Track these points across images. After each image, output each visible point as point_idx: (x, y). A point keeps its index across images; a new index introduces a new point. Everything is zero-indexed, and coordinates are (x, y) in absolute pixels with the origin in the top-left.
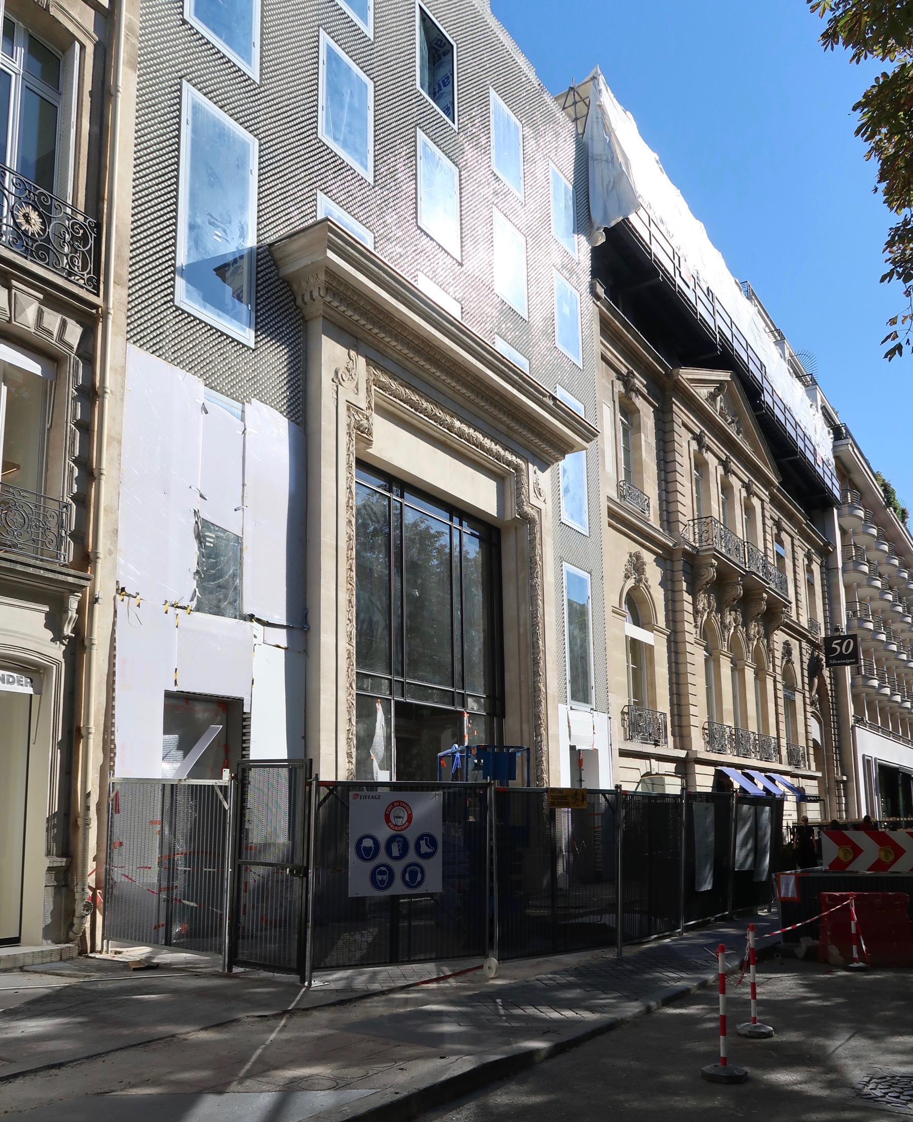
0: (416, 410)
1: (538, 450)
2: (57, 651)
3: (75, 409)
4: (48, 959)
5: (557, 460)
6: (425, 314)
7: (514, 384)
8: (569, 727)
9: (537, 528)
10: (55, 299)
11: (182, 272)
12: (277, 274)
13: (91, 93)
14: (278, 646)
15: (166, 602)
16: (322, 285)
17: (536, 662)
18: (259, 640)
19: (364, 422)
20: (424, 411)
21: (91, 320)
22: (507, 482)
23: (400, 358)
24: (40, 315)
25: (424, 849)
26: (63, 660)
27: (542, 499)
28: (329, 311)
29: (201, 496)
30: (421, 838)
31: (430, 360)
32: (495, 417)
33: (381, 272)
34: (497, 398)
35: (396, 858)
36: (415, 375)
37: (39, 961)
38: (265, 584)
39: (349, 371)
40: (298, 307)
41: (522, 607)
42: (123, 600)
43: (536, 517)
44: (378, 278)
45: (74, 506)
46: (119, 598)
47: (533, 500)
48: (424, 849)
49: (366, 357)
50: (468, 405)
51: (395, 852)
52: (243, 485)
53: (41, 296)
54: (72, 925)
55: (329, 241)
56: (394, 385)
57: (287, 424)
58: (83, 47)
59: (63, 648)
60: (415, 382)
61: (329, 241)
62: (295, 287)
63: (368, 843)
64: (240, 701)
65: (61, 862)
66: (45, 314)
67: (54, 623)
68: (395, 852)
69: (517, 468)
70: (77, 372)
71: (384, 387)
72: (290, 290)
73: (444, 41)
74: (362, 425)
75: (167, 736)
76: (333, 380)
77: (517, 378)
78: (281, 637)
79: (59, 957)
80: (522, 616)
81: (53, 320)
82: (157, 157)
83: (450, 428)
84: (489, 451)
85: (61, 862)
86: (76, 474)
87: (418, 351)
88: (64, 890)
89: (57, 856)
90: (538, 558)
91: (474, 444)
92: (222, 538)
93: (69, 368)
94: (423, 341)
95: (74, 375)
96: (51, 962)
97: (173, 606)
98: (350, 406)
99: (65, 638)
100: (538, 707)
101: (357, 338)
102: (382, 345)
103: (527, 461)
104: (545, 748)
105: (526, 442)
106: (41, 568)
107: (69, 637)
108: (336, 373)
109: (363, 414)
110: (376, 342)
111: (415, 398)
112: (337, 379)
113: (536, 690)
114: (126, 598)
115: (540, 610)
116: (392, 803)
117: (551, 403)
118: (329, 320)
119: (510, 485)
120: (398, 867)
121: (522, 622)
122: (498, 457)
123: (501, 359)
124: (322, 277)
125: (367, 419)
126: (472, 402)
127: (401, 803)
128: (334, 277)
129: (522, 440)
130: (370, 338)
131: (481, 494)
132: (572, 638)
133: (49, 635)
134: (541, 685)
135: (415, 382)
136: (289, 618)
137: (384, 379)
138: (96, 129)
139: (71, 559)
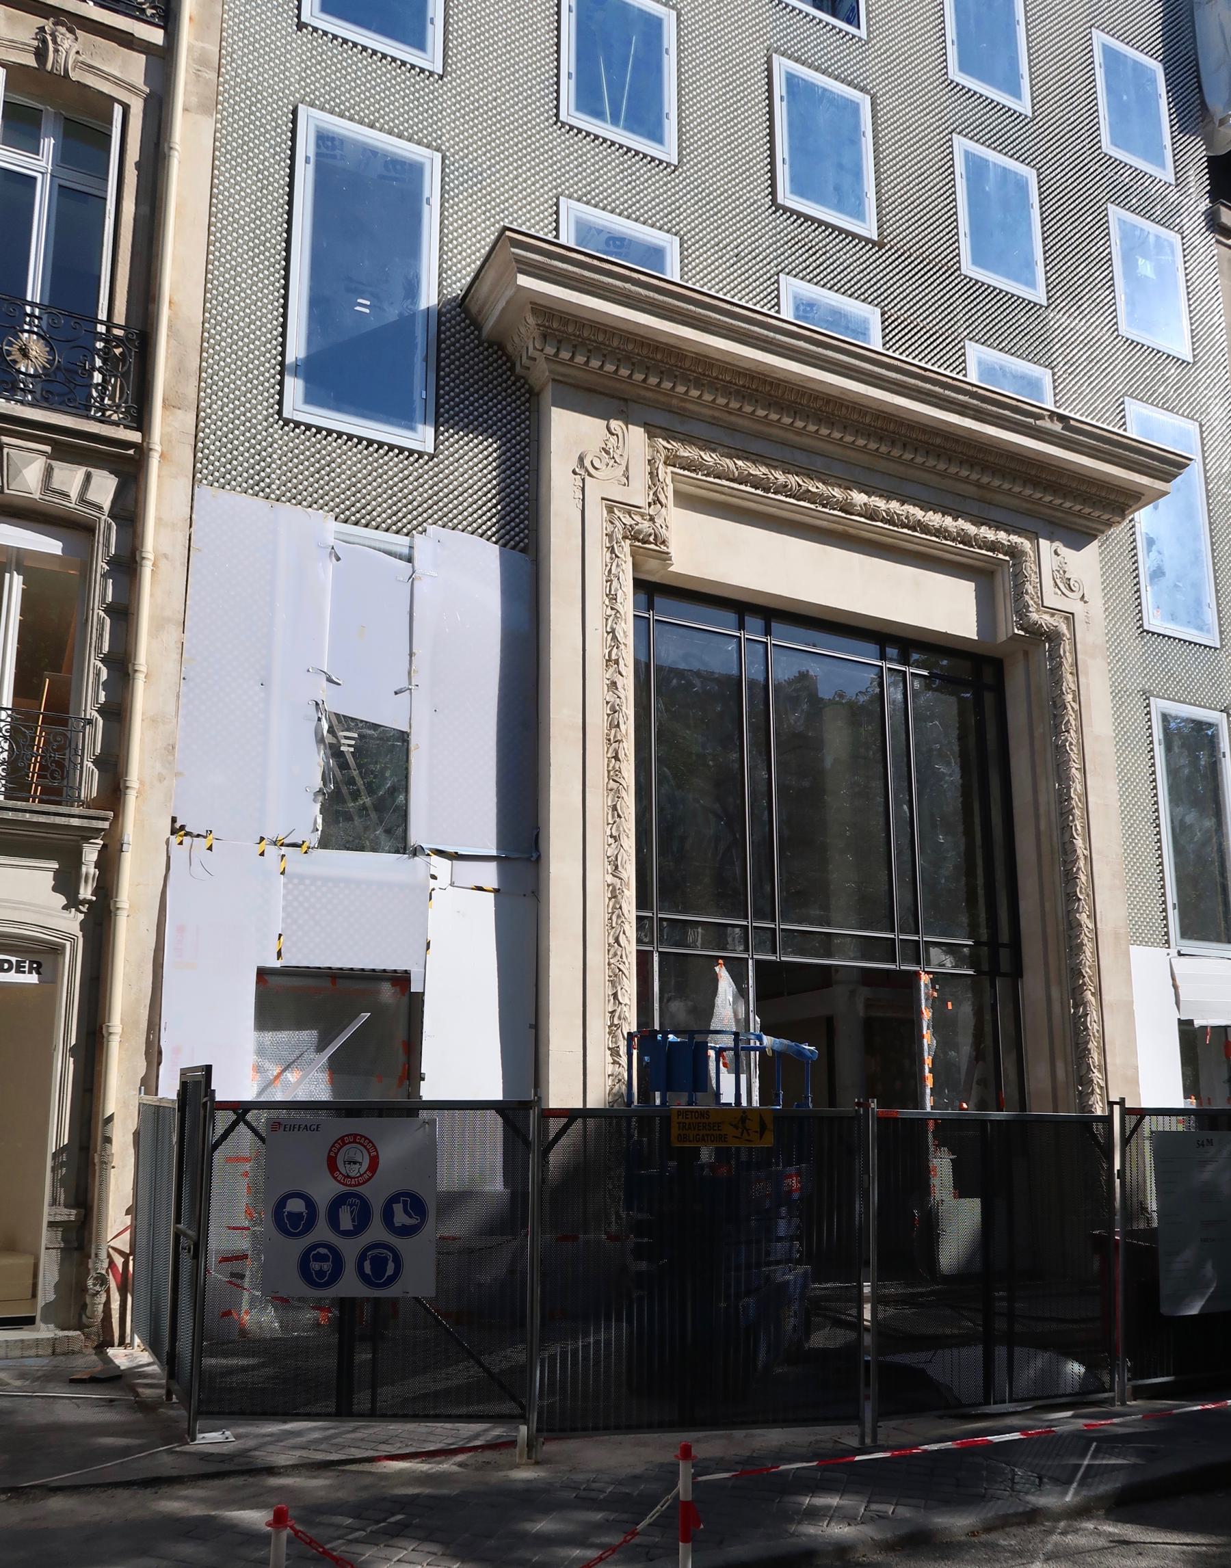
0: (767, 490)
1: (1059, 514)
2: (71, 923)
3: (105, 589)
4: (32, 1352)
5: (1109, 524)
6: (736, 332)
7: (962, 409)
8: (1175, 987)
9: (1066, 647)
10: (68, 448)
11: (297, 370)
12: (477, 338)
13: (138, 165)
14: (480, 889)
15: (262, 839)
16: (536, 333)
17: (1070, 878)
18: (444, 880)
19: (645, 526)
20: (783, 489)
21: (130, 468)
22: (993, 578)
23: (717, 414)
24: (48, 472)
25: (400, 1218)
26: (80, 934)
27: (1078, 595)
29: (330, 680)
30: (394, 1199)
31: (774, 403)
32: (943, 475)
33: (628, 286)
34: (938, 441)
35: (346, 1234)
36: (757, 436)
37: (17, 1353)
39: (607, 453)
40: (518, 378)
41: (1042, 785)
42: (181, 843)
43: (1063, 628)
44: (627, 296)
45: (100, 722)
46: (175, 840)
47: (1052, 600)
48: (400, 1218)
49: (647, 426)
50: (882, 465)
51: (346, 1222)
52: (411, 655)
53: (48, 449)
54: (84, 1306)
55: (517, 261)
56: (709, 458)
57: (498, 553)
58: (126, 108)
59: (82, 916)
61: (517, 261)
62: (510, 349)
63: (296, 1206)
65: (71, 1215)
66: (56, 472)
67: (66, 883)
68: (346, 1222)
69: (1014, 553)
70: (108, 540)
71: (689, 466)
72: (505, 354)
74: (640, 532)
75: (269, 1036)
76: (574, 472)
77: (966, 399)
78: (489, 874)
79: (50, 1351)
80: (1043, 799)
81: (70, 478)
82: (709, 273)
83: (847, 508)
84: (940, 532)
85: (71, 1215)
86: (104, 676)
87: (744, 394)
88: (76, 1255)
89: (66, 1207)
90: (1069, 697)
91: (904, 526)
92: (371, 737)
93: (100, 538)
94: (753, 378)
95: (109, 540)
96: (37, 1356)
97: (275, 843)
98: (611, 505)
99: (83, 902)
100: (1078, 955)
101: (626, 400)
102: (675, 402)
103: (1034, 536)
104: (1094, 1027)
105: (1029, 506)
106: (25, 811)
107: (89, 902)
108: (581, 460)
109: (642, 515)
110: (662, 399)
111: (759, 471)
112: (583, 469)
113: (1073, 927)
114: (187, 840)
115: (1077, 787)
116: (342, 1138)
117: (1057, 427)
118: (560, 382)
119: (1004, 584)
120: (350, 1249)
121: (1042, 810)
122: (966, 539)
124: (531, 320)
125: (652, 519)
126: (888, 457)
127: (355, 1138)
128: (545, 310)
129: (1015, 502)
130: (649, 394)
131: (943, 606)
132: (1180, 830)
133: (62, 900)
134: (1083, 918)
136: (500, 846)
137: (687, 452)
138: (146, 209)
139: (94, 794)
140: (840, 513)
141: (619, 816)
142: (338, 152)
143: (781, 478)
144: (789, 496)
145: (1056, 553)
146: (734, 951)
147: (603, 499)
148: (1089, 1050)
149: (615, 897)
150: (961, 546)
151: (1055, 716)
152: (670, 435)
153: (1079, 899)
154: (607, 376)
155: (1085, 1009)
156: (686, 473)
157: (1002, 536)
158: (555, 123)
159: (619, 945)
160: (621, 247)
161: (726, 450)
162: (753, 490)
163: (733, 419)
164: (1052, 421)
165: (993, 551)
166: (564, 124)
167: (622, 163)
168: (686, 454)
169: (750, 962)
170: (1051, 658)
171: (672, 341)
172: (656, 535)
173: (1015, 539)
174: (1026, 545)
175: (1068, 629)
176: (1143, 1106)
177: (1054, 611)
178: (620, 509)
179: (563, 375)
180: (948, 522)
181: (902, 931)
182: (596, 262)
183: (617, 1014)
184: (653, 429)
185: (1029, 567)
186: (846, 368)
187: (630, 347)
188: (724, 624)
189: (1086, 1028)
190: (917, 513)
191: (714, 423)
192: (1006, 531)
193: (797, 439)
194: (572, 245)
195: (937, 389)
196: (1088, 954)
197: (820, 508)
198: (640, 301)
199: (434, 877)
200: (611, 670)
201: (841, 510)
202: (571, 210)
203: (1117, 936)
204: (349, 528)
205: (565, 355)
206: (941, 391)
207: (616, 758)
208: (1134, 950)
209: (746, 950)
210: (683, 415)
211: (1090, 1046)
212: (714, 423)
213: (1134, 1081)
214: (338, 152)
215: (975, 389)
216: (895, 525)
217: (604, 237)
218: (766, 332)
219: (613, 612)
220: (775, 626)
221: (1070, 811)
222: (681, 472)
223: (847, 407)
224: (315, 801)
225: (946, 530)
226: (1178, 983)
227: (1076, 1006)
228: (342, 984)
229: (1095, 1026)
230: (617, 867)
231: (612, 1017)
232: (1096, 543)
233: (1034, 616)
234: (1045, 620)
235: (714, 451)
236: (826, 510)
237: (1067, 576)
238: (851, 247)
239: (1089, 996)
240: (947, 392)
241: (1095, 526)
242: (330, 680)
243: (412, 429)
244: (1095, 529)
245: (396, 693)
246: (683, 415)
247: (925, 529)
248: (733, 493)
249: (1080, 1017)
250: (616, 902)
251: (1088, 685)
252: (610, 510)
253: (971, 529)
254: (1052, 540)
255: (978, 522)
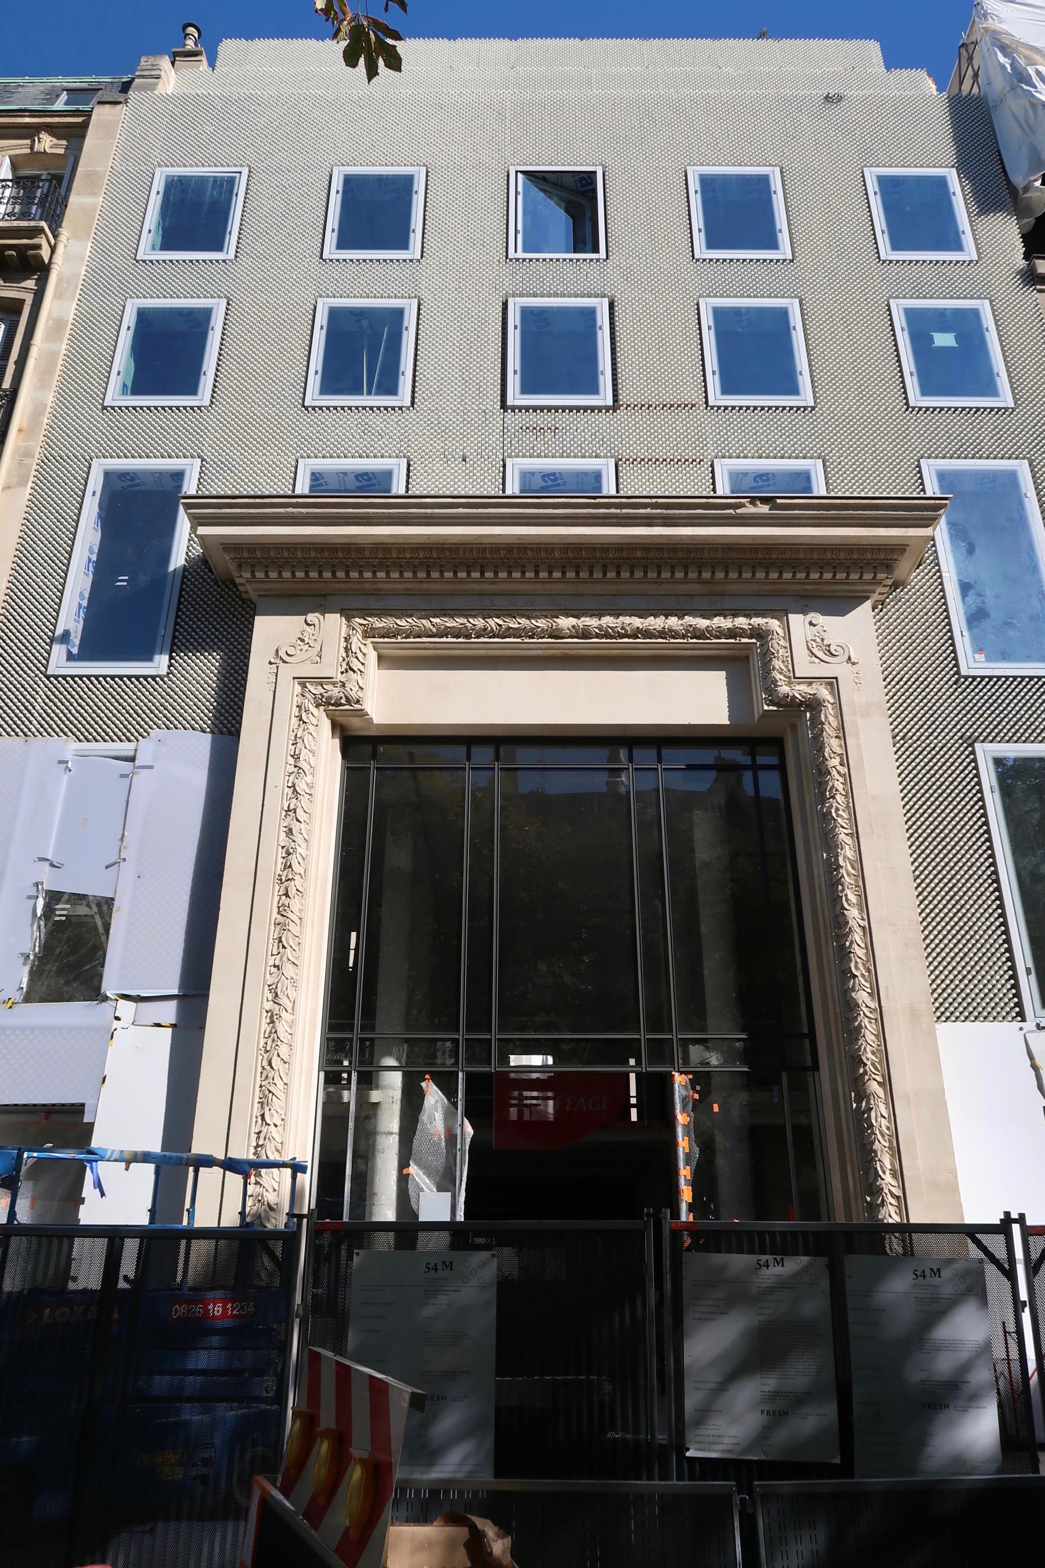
7: (649, 521)
8: (1035, 1067)
9: (828, 715)
14: (158, 1025)
19: (335, 692)
20: (483, 632)
22: (743, 664)
23: (409, 586)
28: (262, 586)
33: (290, 510)
36: (453, 594)
38: (143, 949)
39: (302, 640)
43: (824, 693)
44: (292, 518)
47: (804, 667)
60: (450, 604)
64: (78, 1109)
69: (761, 635)
71: (387, 634)
73: (585, 176)
74: (330, 698)
98: (303, 681)
101: (325, 596)
102: (367, 586)
103: (781, 614)
117: (764, 509)
123: (655, 502)
131: (697, 699)
134: (862, 997)
135: (450, 604)
136: (180, 988)
137: (378, 623)
140: (550, 640)
141: (284, 947)
142: (321, 481)
143: (479, 622)
144: (494, 636)
145: (811, 624)
146: (444, 1065)
147: (294, 678)
148: (875, 1152)
149: (272, 1022)
150: (694, 641)
151: (820, 783)
152: (365, 613)
153: (855, 976)
154: (301, 581)
155: (868, 1102)
156: (386, 640)
157: (741, 622)
158: (907, 410)
159: (272, 1067)
160: (768, 479)
161: (423, 613)
162: (455, 640)
163: (425, 586)
164: (755, 505)
165: (735, 637)
166: (914, 408)
167: (967, 421)
168: (382, 625)
169: (460, 1074)
170: (814, 726)
171: (346, 541)
172: (346, 697)
173: (757, 621)
174: (774, 624)
175: (832, 693)
176: (967, 1222)
177: (810, 680)
178: (312, 684)
179: (264, 590)
180: (673, 622)
181: (350, 1028)
182: (258, 501)
183: (262, 1135)
184: (348, 612)
185: (777, 644)
186: (512, 518)
187: (326, 554)
188: (597, 757)
189: (871, 1126)
190: (637, 622)
191: (409, 593)
192: (746, 616)
193: (494, 587)
194: (518, 493)
195: (613, 511)
196: (870, 1037)
197: (672, 641)
198: (304, 518)
199: (118, 1019)
200: (289, 818)
201: (550, 637)
202: (930, 468)
203: (914, 1014)
204: (85, 745)
205: (706, 575)
206: (618, 511)
207: (287, 895)
208: (946, 1030)
209: (456, 1063)
210: (378, 594)
211: (877, 1146)
212: (409, 593)
213: (952, 1189)
214: (559, 481)
215: (654, 500)
216: (612, 637)
217: (750, 478)
218: (423, 511)
219: (296, 770)
220: (665, 752)
221: (840, 881)
222: (382, 640)
223: (532, 550)
224: (24, 964)
225: (671, 630)
226: (1038, 1061)
227: (859, 1101)
228: (54, 1118)
229: (884, 1123)
230: (277, 995)
231: (258, 1138)
232: (868, 604)
233: (784, 689)
234: (800, 691)
235: (411, 616)
236: (535, 640)
237: (825, 643)
238: (594, 417)
239: (874, 1087)
240: (624, 511)
241: (859, 588)
242: (52, 865)
243: (151, 659)
244: (866, 591)
245: (107, 867)
246: (378, 594)
247: (647, 634)
248: (435, 646)
249: (864, 1113)
250: (273, 1027)
251: (859, 746)
252: (303, 686)
253: (702, 623)
254: (805, 612)
255: (708, 613)
